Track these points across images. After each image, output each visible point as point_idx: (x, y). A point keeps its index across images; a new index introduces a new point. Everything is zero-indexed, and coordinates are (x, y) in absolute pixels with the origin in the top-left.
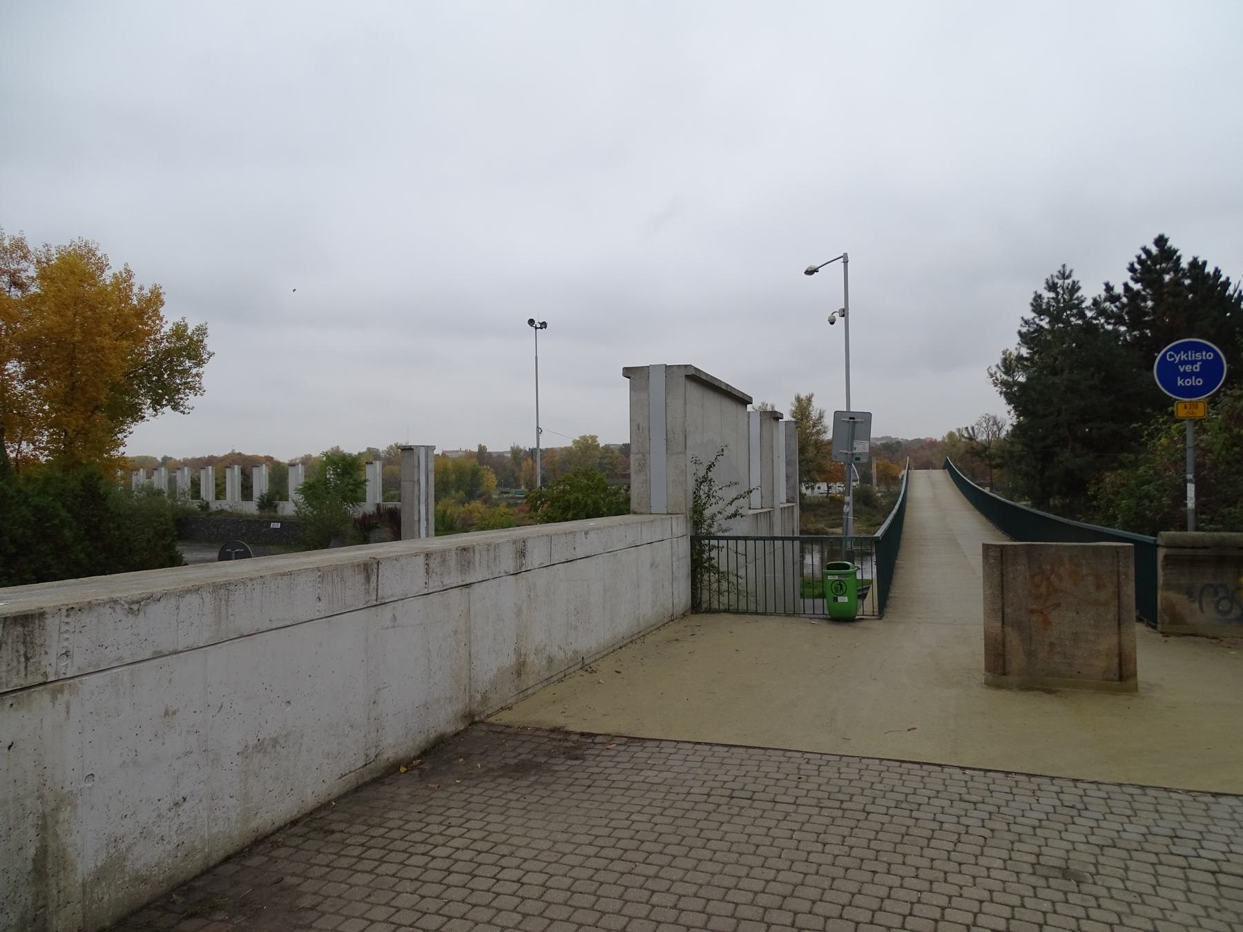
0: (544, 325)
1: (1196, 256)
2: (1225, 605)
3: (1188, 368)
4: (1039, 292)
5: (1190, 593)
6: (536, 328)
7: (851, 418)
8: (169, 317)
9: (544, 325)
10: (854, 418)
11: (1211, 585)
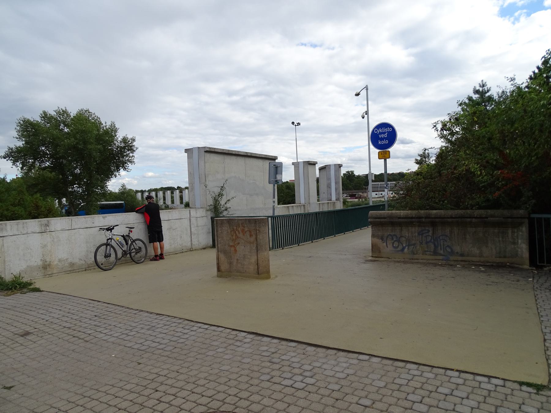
0: (299, 124)
1: (533, 71)
2: (396, 244)
3: (382, 136)
4: (470, 95)
5: (382, 239)
6: (296, 126)
7: (274, 165)
8: (120, 136)
9: (299, 124)
10: (275, 165)
11: (390, 235)
